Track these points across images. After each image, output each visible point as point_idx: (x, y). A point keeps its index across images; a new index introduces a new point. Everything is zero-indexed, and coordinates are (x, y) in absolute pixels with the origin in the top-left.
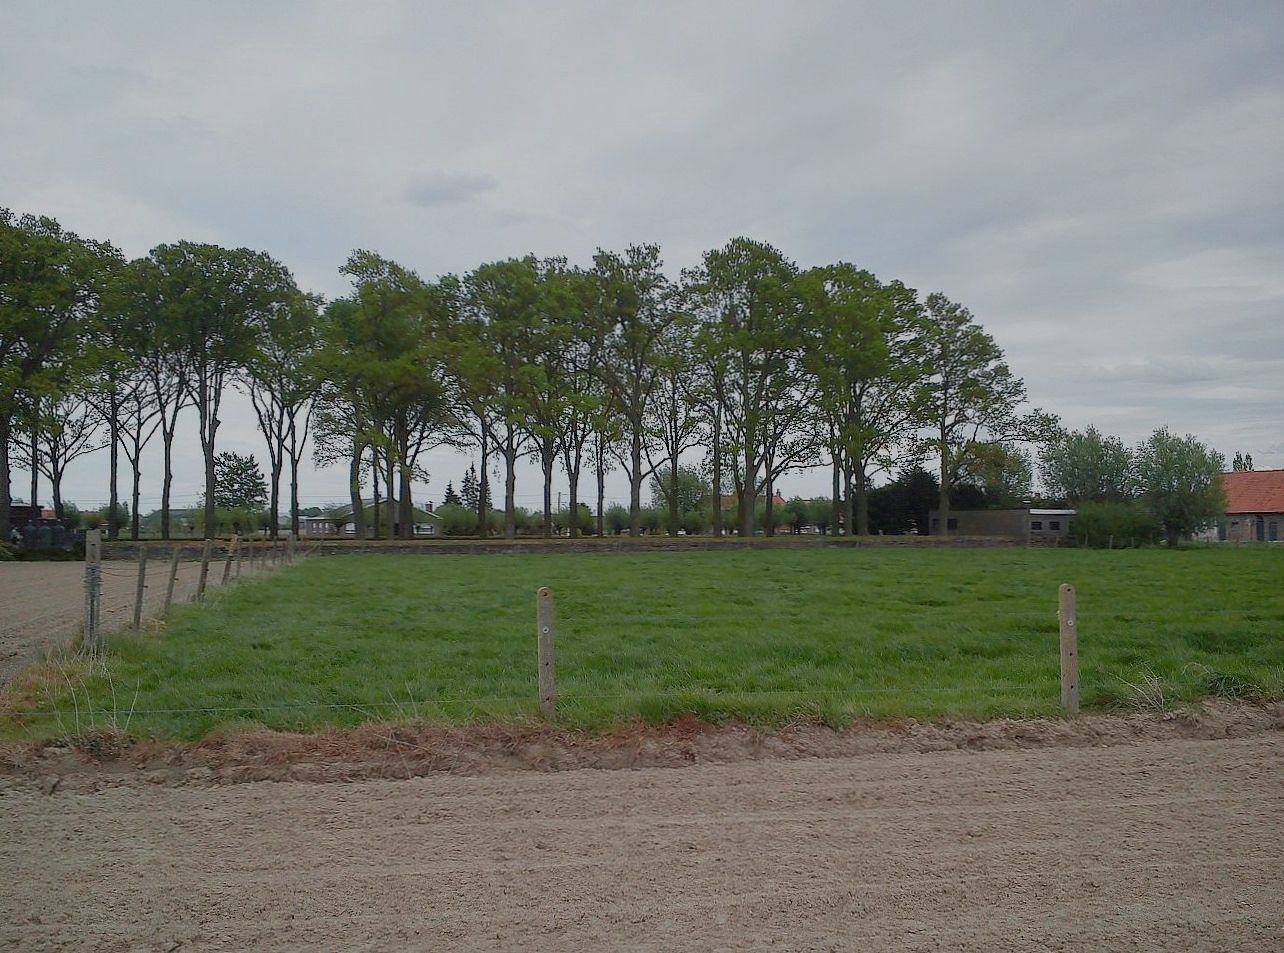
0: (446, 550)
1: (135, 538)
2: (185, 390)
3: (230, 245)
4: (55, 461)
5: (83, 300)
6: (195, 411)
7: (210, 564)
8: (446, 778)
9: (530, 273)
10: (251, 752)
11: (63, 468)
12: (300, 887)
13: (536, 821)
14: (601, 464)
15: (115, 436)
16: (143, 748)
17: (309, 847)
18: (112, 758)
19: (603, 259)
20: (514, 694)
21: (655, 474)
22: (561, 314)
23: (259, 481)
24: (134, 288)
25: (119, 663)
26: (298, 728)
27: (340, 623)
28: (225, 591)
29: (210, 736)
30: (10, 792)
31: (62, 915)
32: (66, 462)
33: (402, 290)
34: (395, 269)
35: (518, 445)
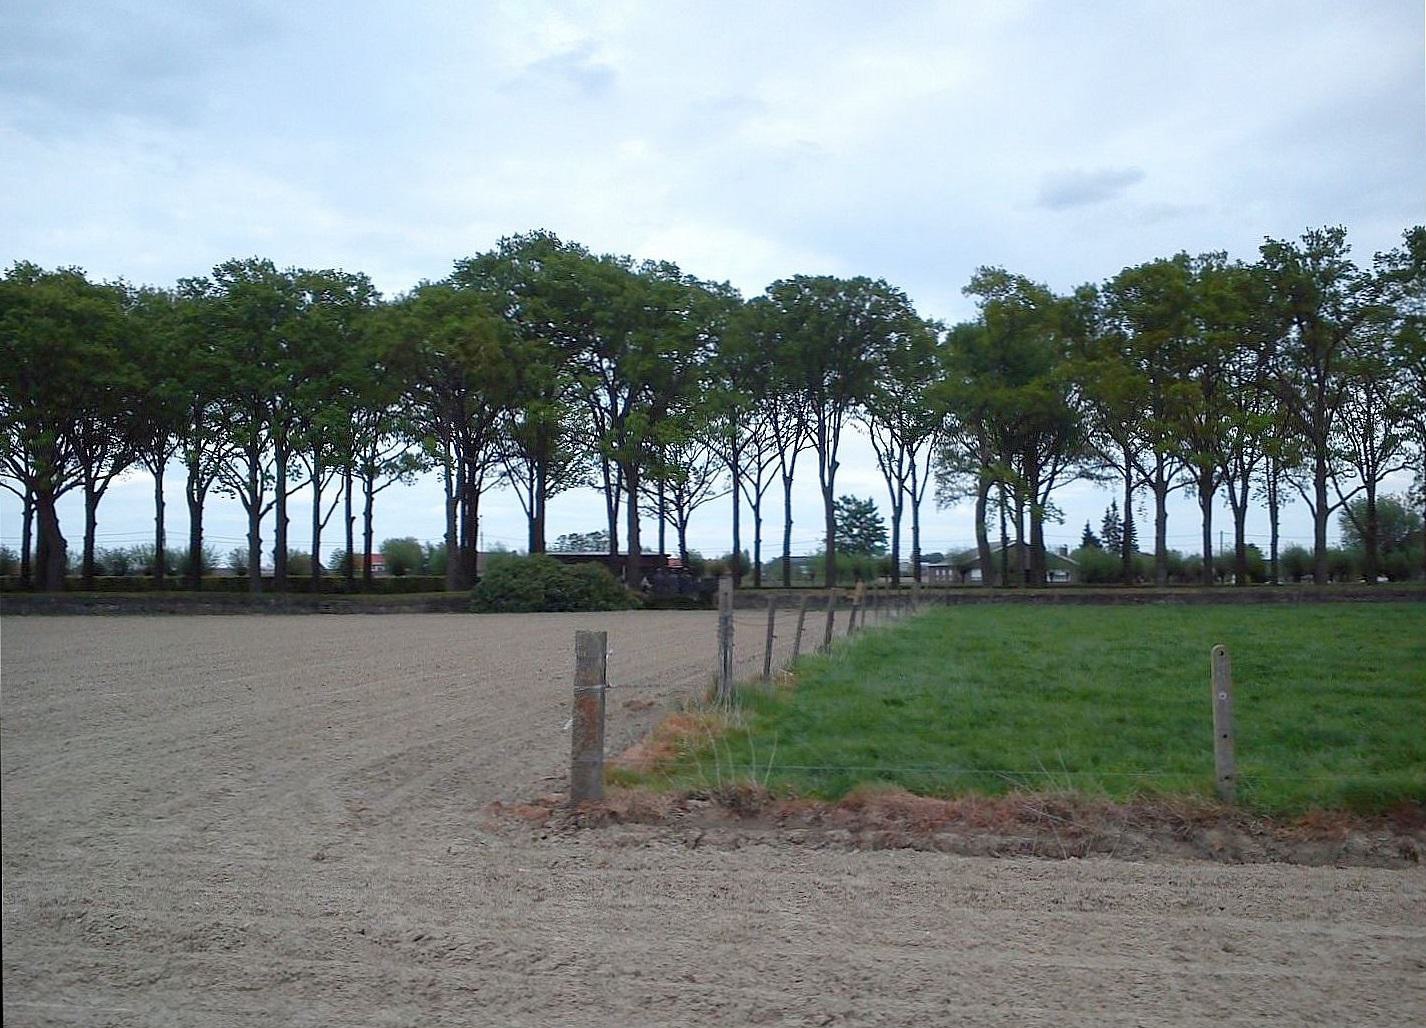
0: (1085, 600)
1: (757, 586)
2: (803, 432)
3: (845, 274)
4: (680, 509)
5: (703, 344)
6: (814, 453)
7: (835, 614)
8: (1107, 862)
9: (1182, 273)
10: (892, 817)
11: (688, 515)
12: (954, 969)
13: (1220, 919)
14: (1275, 495)
15: (737, 483)
16: (782, 805)
17: (961, 926)
18: (753, 814)
19: (1272, 250)
20: (1183, 770)
21: (1346, 506)
22: (1222, 318)
23: (878, 525)
24: (752, 327)
25: (754, 715)
26: (939, 794)
27: (975, 680)
28: (851, 642)
29: (849, 797)
30: (656, 844)
31: (714, 975)
32: (691, 509)
33: (1033, 307)
34: (1023, 284)
35: (1170, 477)
